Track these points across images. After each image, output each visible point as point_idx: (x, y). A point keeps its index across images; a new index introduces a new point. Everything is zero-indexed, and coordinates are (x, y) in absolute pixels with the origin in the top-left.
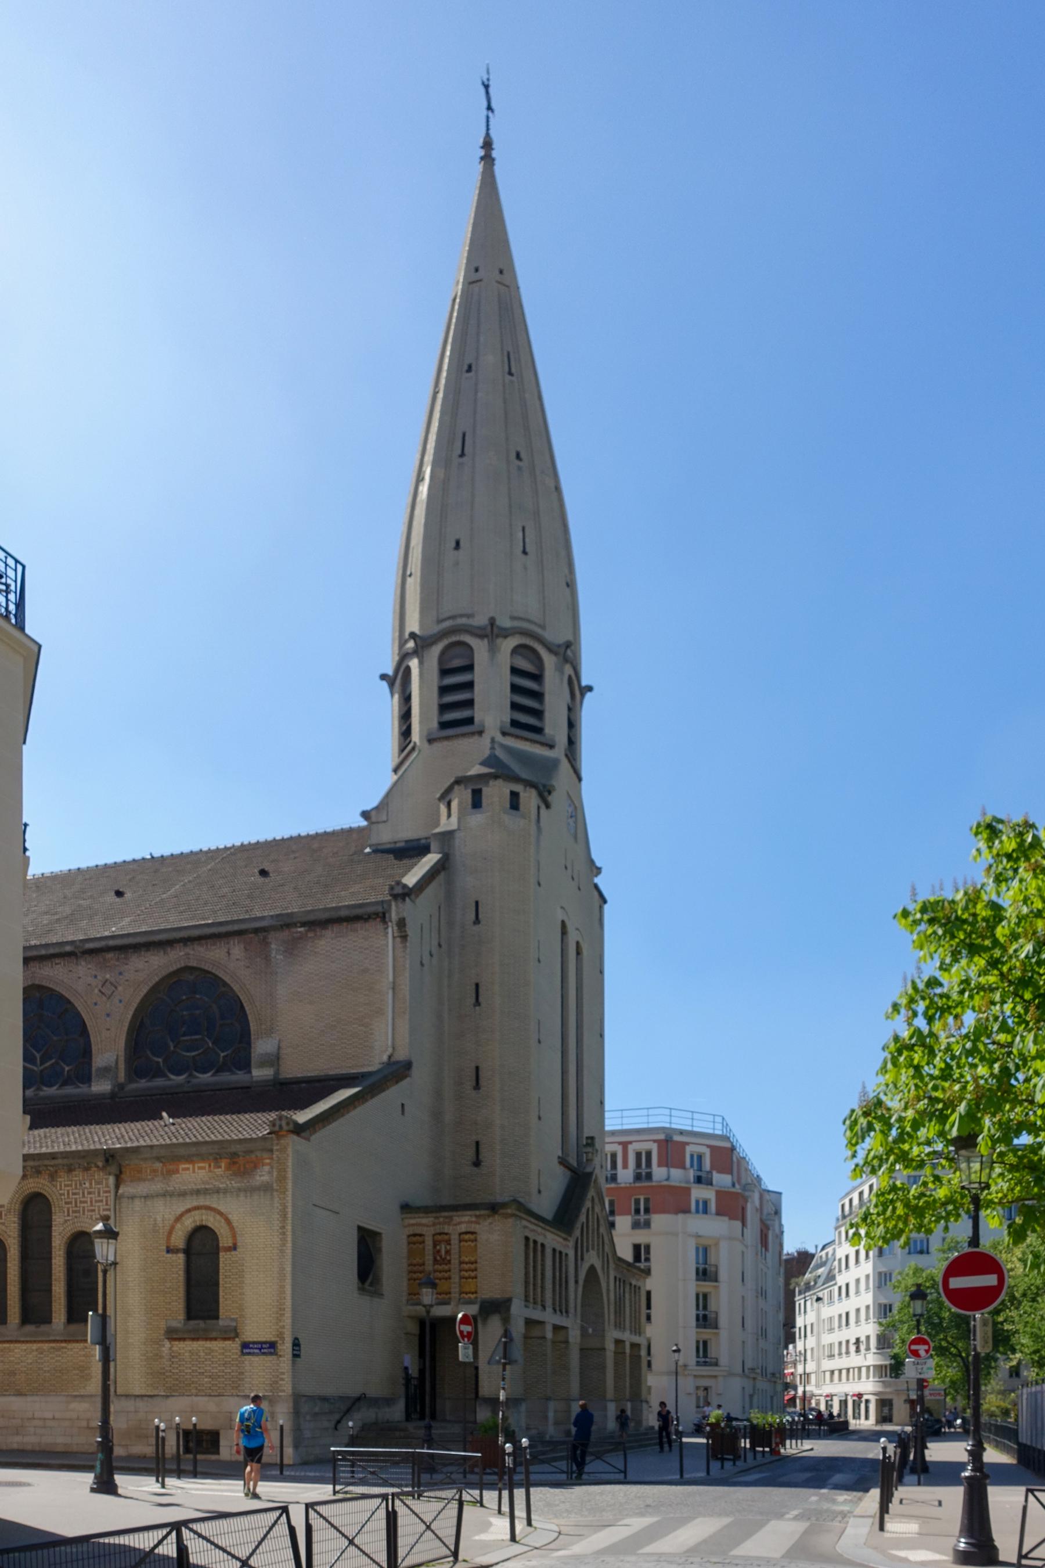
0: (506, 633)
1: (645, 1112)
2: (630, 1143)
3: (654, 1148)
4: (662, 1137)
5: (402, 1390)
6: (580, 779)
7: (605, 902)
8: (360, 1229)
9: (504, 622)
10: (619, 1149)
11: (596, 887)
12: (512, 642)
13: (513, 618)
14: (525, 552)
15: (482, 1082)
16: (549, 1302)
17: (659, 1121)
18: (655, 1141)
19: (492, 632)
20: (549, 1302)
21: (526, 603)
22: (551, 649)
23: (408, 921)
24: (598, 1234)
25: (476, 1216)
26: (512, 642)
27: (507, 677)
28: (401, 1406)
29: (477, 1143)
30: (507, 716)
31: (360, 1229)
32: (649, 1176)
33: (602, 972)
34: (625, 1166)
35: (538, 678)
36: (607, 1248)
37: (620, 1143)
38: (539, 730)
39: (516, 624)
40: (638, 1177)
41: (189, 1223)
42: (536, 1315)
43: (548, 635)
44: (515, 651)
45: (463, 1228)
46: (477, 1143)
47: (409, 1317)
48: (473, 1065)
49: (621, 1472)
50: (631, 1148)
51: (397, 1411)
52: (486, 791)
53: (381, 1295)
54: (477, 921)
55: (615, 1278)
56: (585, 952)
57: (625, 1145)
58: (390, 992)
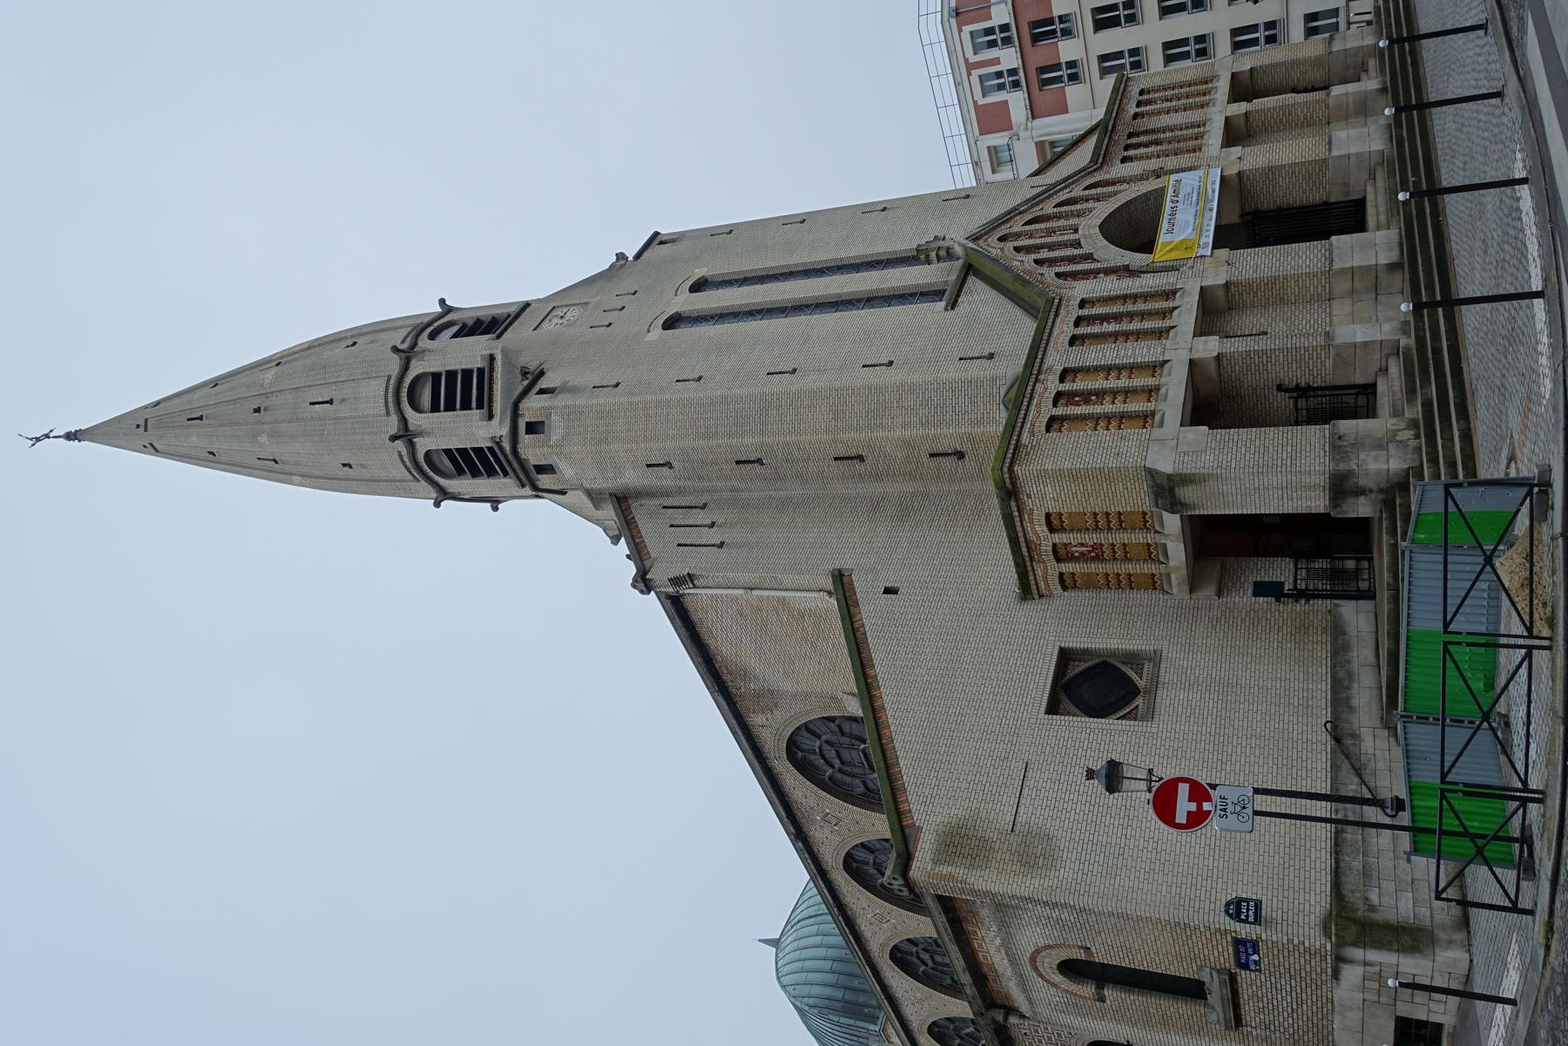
0: (404, 420)
1: (928, 49)
2: (966, 60)
3: (967, 29)
4: (953, 21)
5: (1322, 605)
6: (527, 305)
7: (656, 234)
8: (1053, 708)
9: (393, 425)
10: (976, 73)
11: (638, 256)
12: (409, 413)
13: (388, 414)
14: (330, 402)
15: (853, 452)
16: (1195, 116)
17: (934, 28)
18: (960, 31)
19: (406, 434)
20: (1195, 116)
21: (372, 396)
22: (405, 369)
23: (671, 576)
24: (1058, 217)
25: (1020, 515)
26: (409, 413)
27: (444, 417)
28: (1348, 609)
29: (932, 455)
30: (475, 414)
31: (1053, 708)
32: (1005, 28)
33: (730, 230)
34: (996, 61)
35: (436, 377)
36: (1077, 191)
37: (969, 74)
38: (481, 371)
39: (392, 408)
40: (1007, 41)
41: (1058, 978)
42: (1223, 87)
43: (395, 371)
44: (416, 407)
45: (1042, 529)
46: (932, 455)
47: (1191, 592)
48: (834, 463)
49: (1529, 656)
50: (973, 59)
51: (1357, 617)
52: (533, 461)
53: (1156, 658)
54: (668, 465)
55: (1124, 160)
56: (700, 272)
57: (970, 67)
58: (755, 593)
